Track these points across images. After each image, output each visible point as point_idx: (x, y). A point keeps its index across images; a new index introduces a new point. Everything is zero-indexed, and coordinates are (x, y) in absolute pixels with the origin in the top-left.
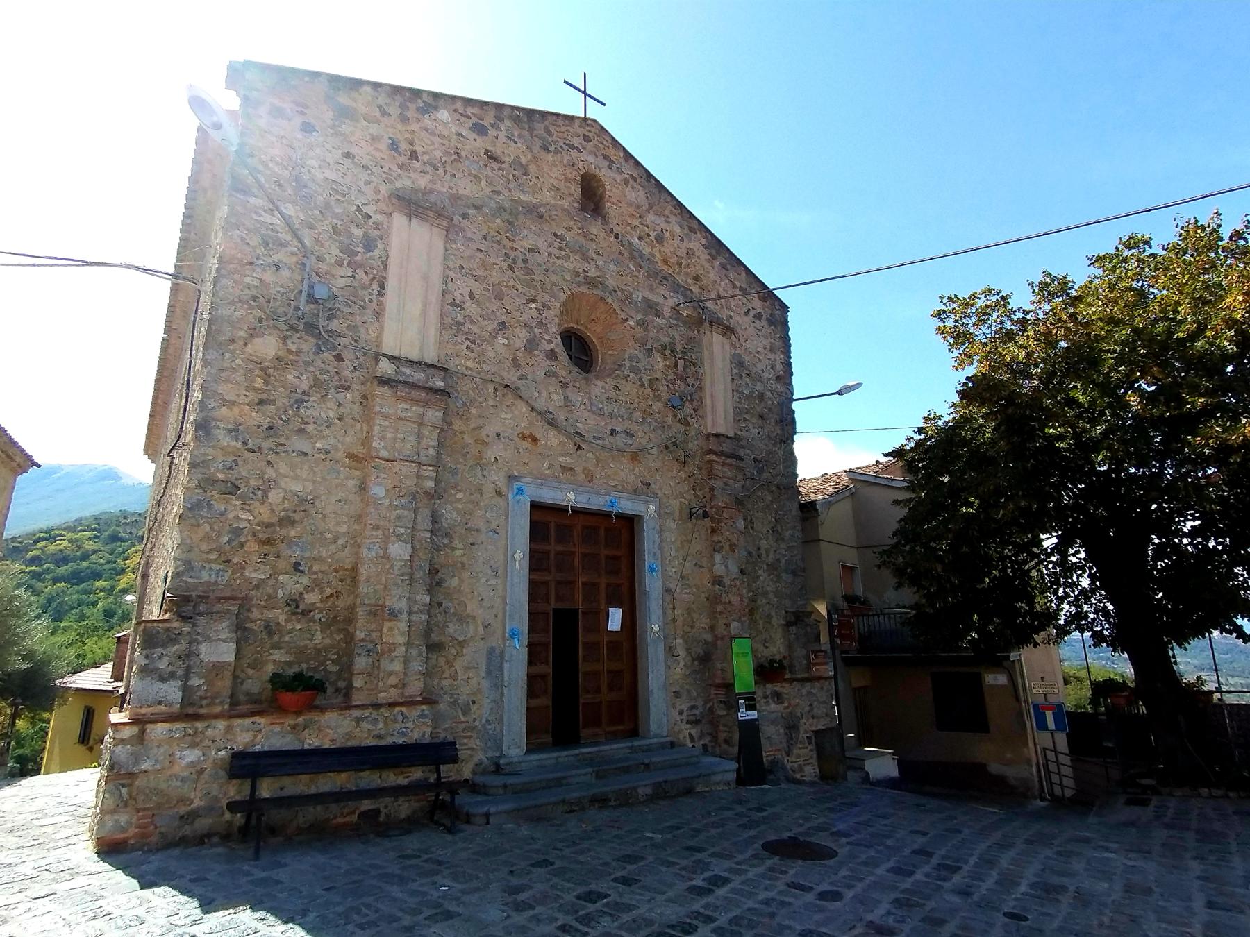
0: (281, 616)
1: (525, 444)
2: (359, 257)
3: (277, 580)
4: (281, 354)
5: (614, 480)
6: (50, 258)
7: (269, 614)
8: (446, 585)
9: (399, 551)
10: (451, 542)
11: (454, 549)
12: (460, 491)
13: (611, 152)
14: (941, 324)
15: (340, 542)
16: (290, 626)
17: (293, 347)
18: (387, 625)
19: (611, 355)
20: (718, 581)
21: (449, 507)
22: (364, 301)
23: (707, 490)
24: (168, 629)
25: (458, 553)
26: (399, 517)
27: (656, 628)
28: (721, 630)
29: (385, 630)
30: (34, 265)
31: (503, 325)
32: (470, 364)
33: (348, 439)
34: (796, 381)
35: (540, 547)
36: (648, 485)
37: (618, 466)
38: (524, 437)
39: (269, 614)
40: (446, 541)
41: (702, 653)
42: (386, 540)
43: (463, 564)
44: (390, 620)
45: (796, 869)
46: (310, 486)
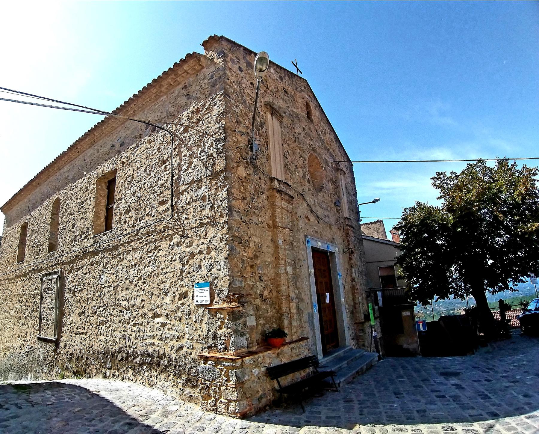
6: (85, 108)
13: (311, 94)
14: (434, 182)
19: (316, 182)
22: (263, 152)
23: (346, 241)
24: (239, 311)
27: (343, 300)
30: (51, 107)
34: (358, 195)
45: (517, 407)
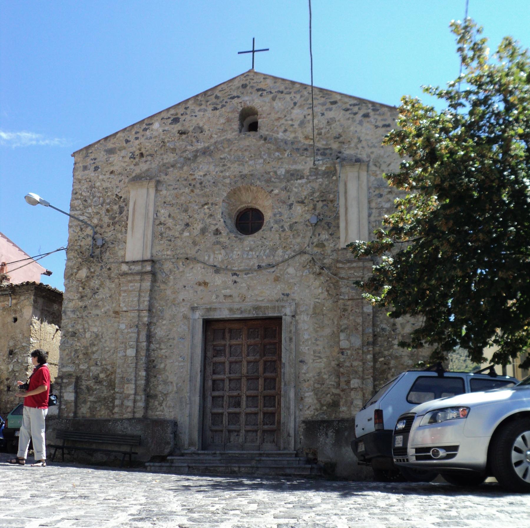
0: (91, 383)
1: (202, 288)
2: (117, 219)
3: (90, 369)
4: (88, 274)
5: (261, 296)
7: (88, 383)
8: (157, 367)
9: (131, 352)
10: (160, 346)
11: (161, 349)
12: (165, 320)
15: (112, 351)
16: (94, 387)
17: (92, 270)
18: (126, 386)
20: (342, 352)
21: (159, 329)
25: (164, 351)
26: (131, 337)
28: (343, 385)
29: (125, 387)
31: (187, 225)
32: (169, 253)
33: (114, 305)
35: (467, 386)
36: (288, 295)
37: (264, 287)
38: (200, 284)
39: (88, 383)
40: (157, 346)
41: (331, 401)
42: (126, 349)
43: (166, 357)
44: (127, 384)
46: (100, 329)
